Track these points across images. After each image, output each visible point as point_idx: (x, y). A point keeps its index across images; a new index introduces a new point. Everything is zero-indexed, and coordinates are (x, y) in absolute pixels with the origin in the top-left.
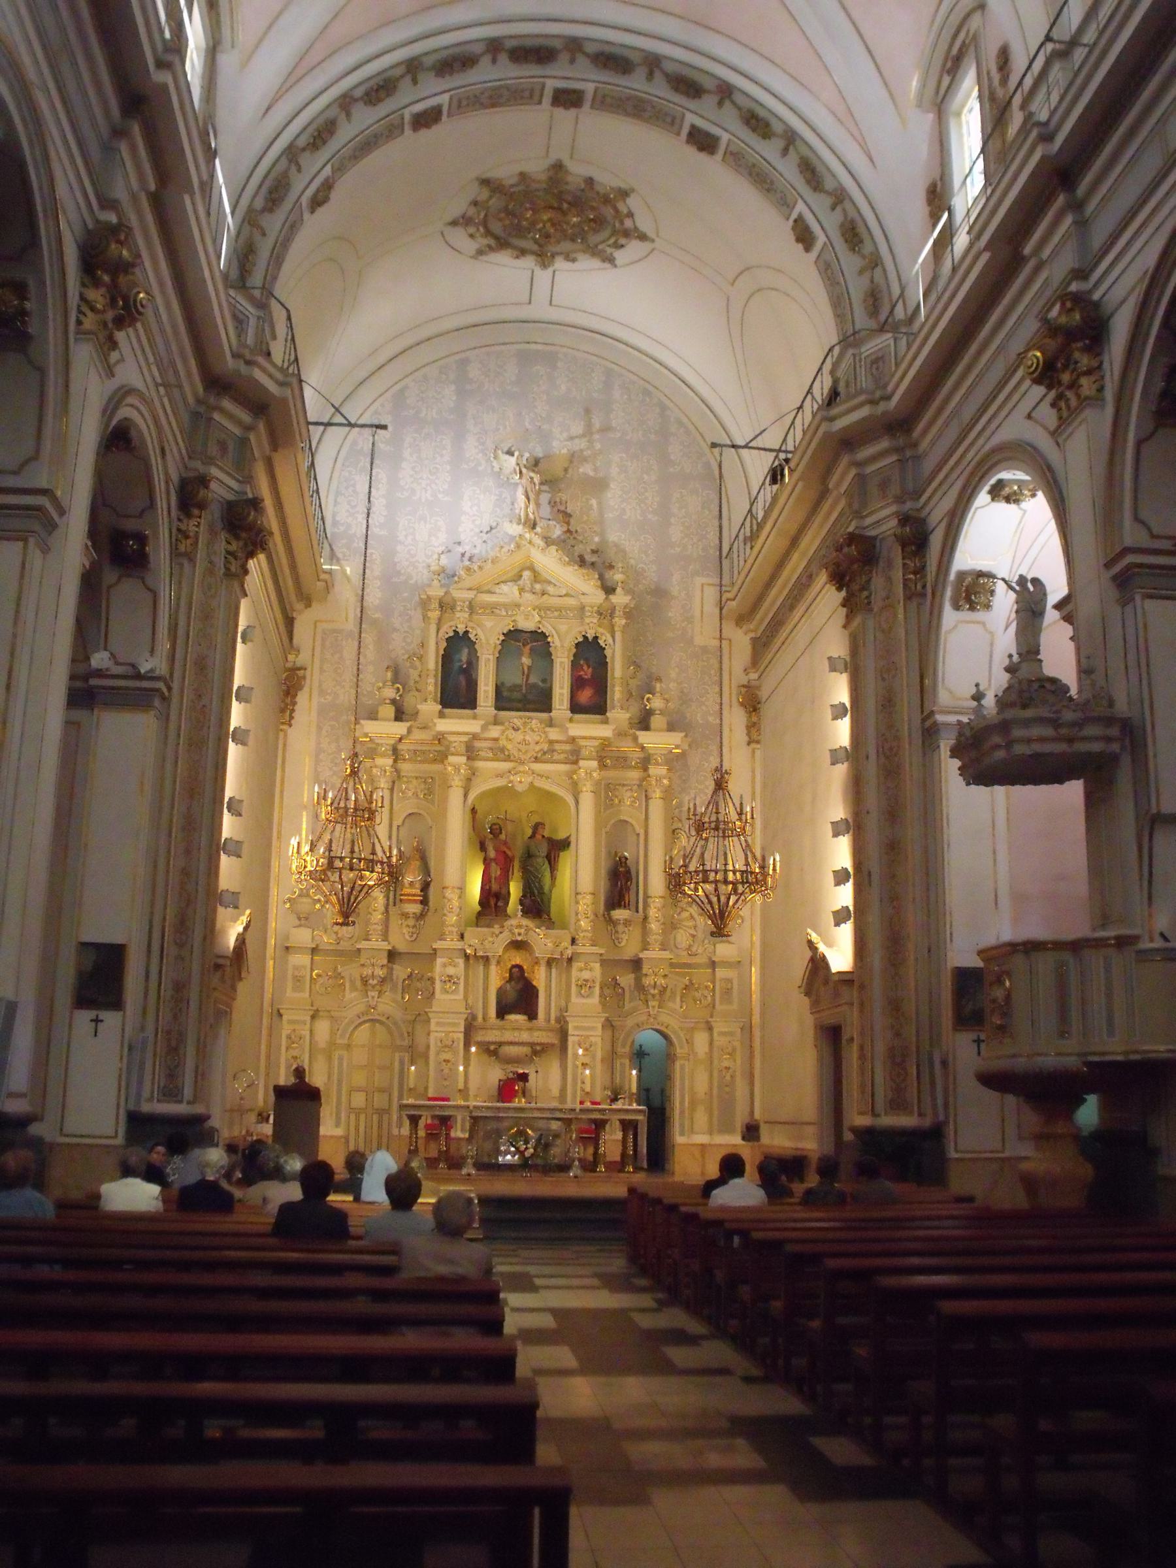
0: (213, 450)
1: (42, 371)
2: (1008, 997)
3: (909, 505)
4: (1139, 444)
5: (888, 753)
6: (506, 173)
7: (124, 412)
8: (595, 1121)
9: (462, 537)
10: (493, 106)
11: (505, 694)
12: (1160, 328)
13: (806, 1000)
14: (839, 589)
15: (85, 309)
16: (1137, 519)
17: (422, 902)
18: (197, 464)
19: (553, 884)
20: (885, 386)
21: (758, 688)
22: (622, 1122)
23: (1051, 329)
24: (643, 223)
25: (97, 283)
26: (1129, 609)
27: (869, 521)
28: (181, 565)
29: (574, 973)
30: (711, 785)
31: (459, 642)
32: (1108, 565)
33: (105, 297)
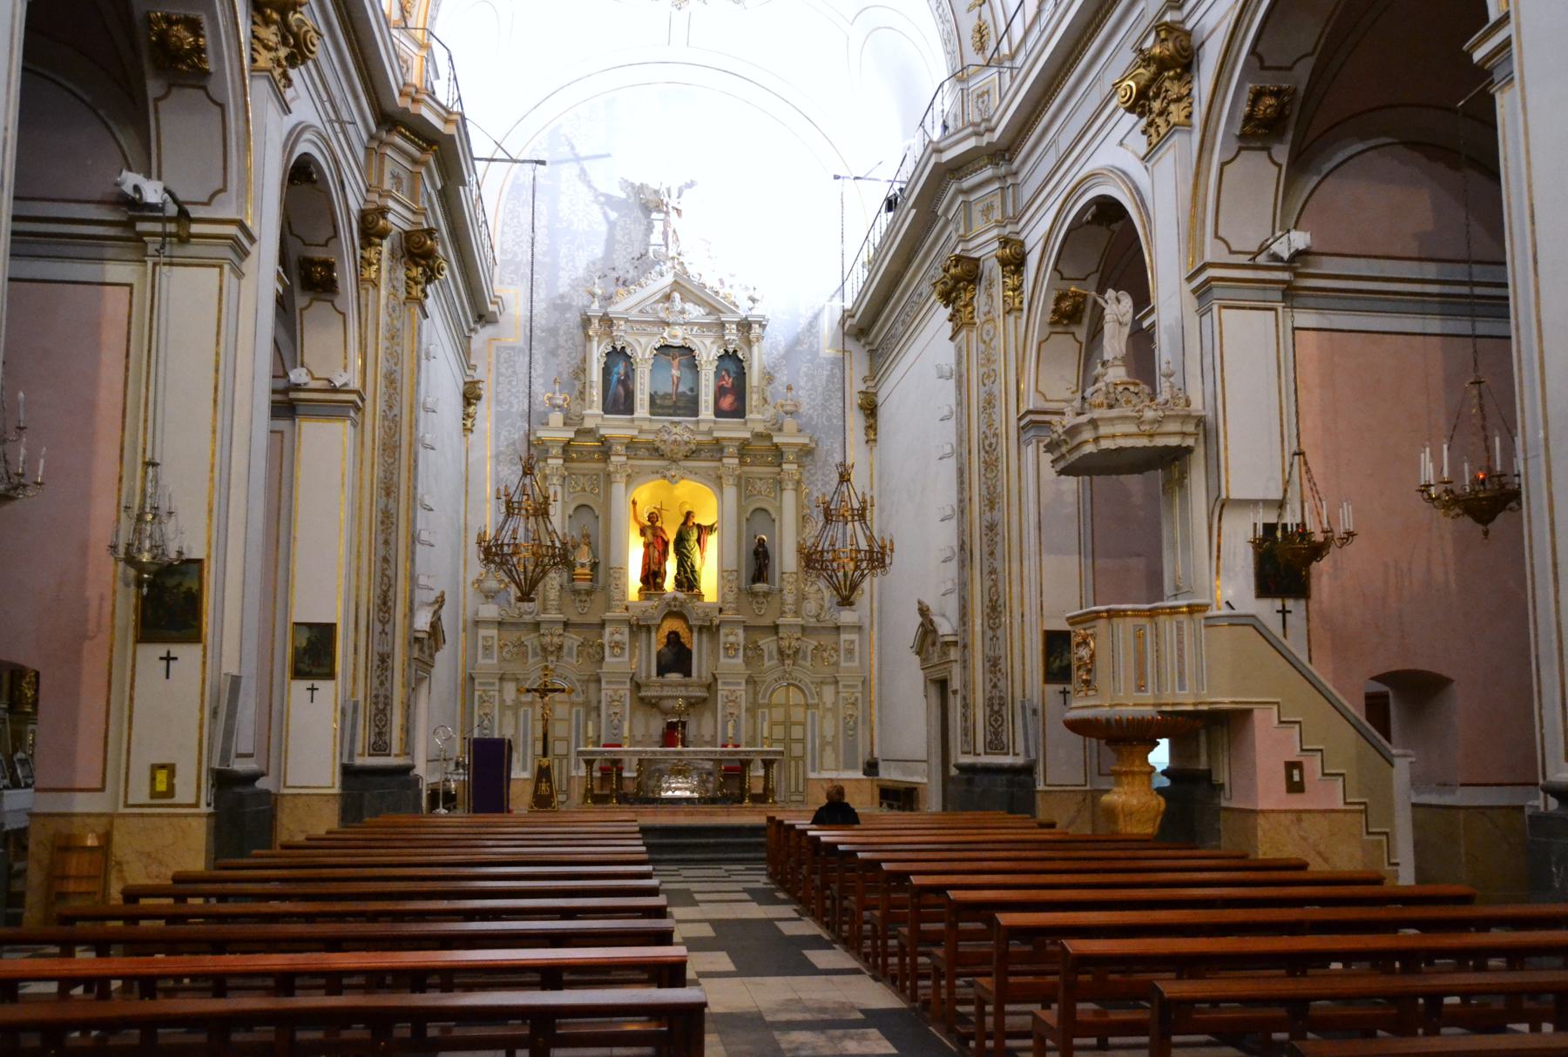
0: (388, 184)
1: (222, 107)
2: (1092, 656)
3: (1009, 228)
4: (1223, 165)
5: (987, 448)
7: (302, 147)
8: (741, 761)
11: (658, 401)
12: (1247, 55)
13: (917, 659)
14: (946, 306)
16: (1217, 236)
17: (591, 580)
18: (375, 197)
19: (703, 563)
20: (989, 120)
21: (876, 394)
23: (1146, 59)
25: (267, 22)
26: (1207, 318)
27: (971, 245)
28: (367, 290)
29: (722, 639)
30: (836, 478)
31: (618, 355)
32: (1190, 279)
33: (276, 35)
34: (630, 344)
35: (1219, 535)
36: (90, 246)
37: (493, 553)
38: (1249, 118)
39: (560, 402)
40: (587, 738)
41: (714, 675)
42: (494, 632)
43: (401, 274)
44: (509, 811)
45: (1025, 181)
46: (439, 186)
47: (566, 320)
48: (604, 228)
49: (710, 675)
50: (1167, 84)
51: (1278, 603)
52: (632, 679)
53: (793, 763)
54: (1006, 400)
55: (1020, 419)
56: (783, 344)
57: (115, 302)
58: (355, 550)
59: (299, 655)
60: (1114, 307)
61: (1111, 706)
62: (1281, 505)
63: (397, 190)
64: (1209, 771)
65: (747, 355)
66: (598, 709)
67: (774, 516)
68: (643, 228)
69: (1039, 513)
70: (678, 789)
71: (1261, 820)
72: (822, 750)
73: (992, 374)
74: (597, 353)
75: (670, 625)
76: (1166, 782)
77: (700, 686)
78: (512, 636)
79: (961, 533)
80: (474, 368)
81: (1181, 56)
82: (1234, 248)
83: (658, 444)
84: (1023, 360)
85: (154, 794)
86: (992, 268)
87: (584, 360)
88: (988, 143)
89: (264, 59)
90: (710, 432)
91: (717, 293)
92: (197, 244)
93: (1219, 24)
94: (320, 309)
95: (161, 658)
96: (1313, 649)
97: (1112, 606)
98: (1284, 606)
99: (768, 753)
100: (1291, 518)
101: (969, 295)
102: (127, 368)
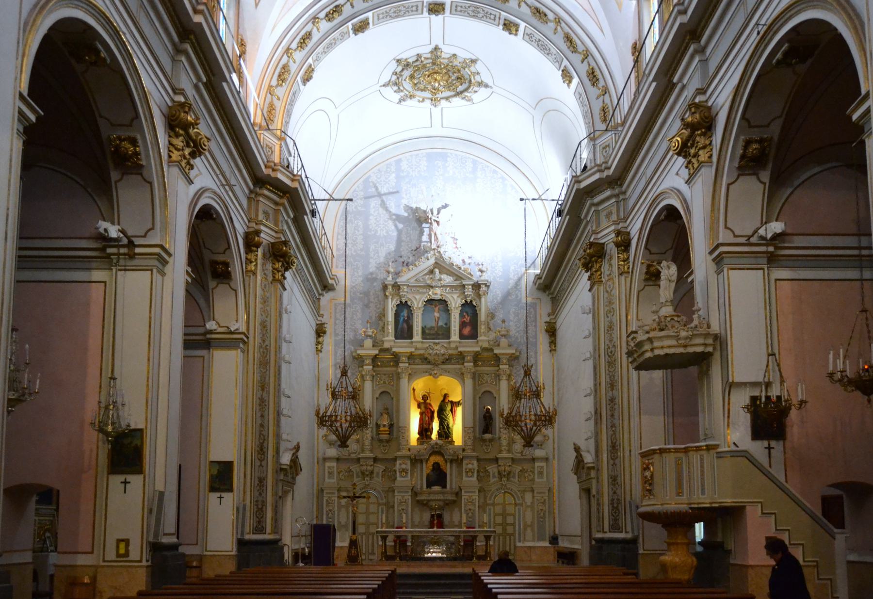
0: (261, 217)
1: (151, 184)
2: (652, 476)
3: (621, 225)
6: (409, 55)
7: (203, 201)
8: (471, 536)
9: (403, 253)
10: (397, 17)
11: (427, 331)
13: (575, 477)
15: (172, 149)
16: (726, 227)
17: (389, 434)
18: (254, 225)
19: (454, 423)
21: (555, 323)
22: (485, 536)
23: (686, 125)
24: (485, 78)
25: (177, 135)
26: (721, 276)
27: (599, 236)
28: (250, 277)
29: (464, 466)
31: (403, 306)
32: (711, 253)
33: (183, 142)
34: (410, 300)
35: (729, 404)
36: (83, 262)
37: (323, 420)
38: (743, 157)
39: (370, 333)
40: (382, 524)
41: (460, 487)
42: (334, 464)
43: (269, 266)
44: (334, 565)
45: (630, 197)
46: (292, 216)
47: (374, 287)
48: (395, 234)
49: (458, 487)
50: (698, 139)
51: (766, 443)
52: (412, 489)
53: (508, 537)
54: (620, 325)
55: (628, 337)
56: (500, 295)
57: (96, 291)
58: (244, 422)
59: (213, 479)
60: (666, 271)
61: (662, 504)
62: (768, 385)
63: (266, 221)
64: (723, 543)
65: (478, 303)
66: (393, 507)
67: (495, 395)
68: (417, 232)
69: (639, 391)
70: (434, 552)
71: (750, 571)
72: (525, 529)
73: (612, 310)
74: (391, 305)
75: (434, 459)
76: (699, 549)
77: (451, 493)
78: (344, 466)
79: (595, 404)
80: (322, 316)
81: (705, 122)
82: (736, 234)
83: (426, 356)
84: (629, 303)
85: (118, 555)
86: (611, 249)
87: (384, 310)
88: (607, 176)
89: (176, 155)
90: (457, 348)
91: (460, 268)
92: (138, 259)
93: (726, 101)
94: (222, 288)
95: (122, 482)
96: (788, 469)
97: (688, 445)
98: (769, 445)
99: (487, 531)
100: (775, 392)
101: (598, 265)
102: (103, 327)
